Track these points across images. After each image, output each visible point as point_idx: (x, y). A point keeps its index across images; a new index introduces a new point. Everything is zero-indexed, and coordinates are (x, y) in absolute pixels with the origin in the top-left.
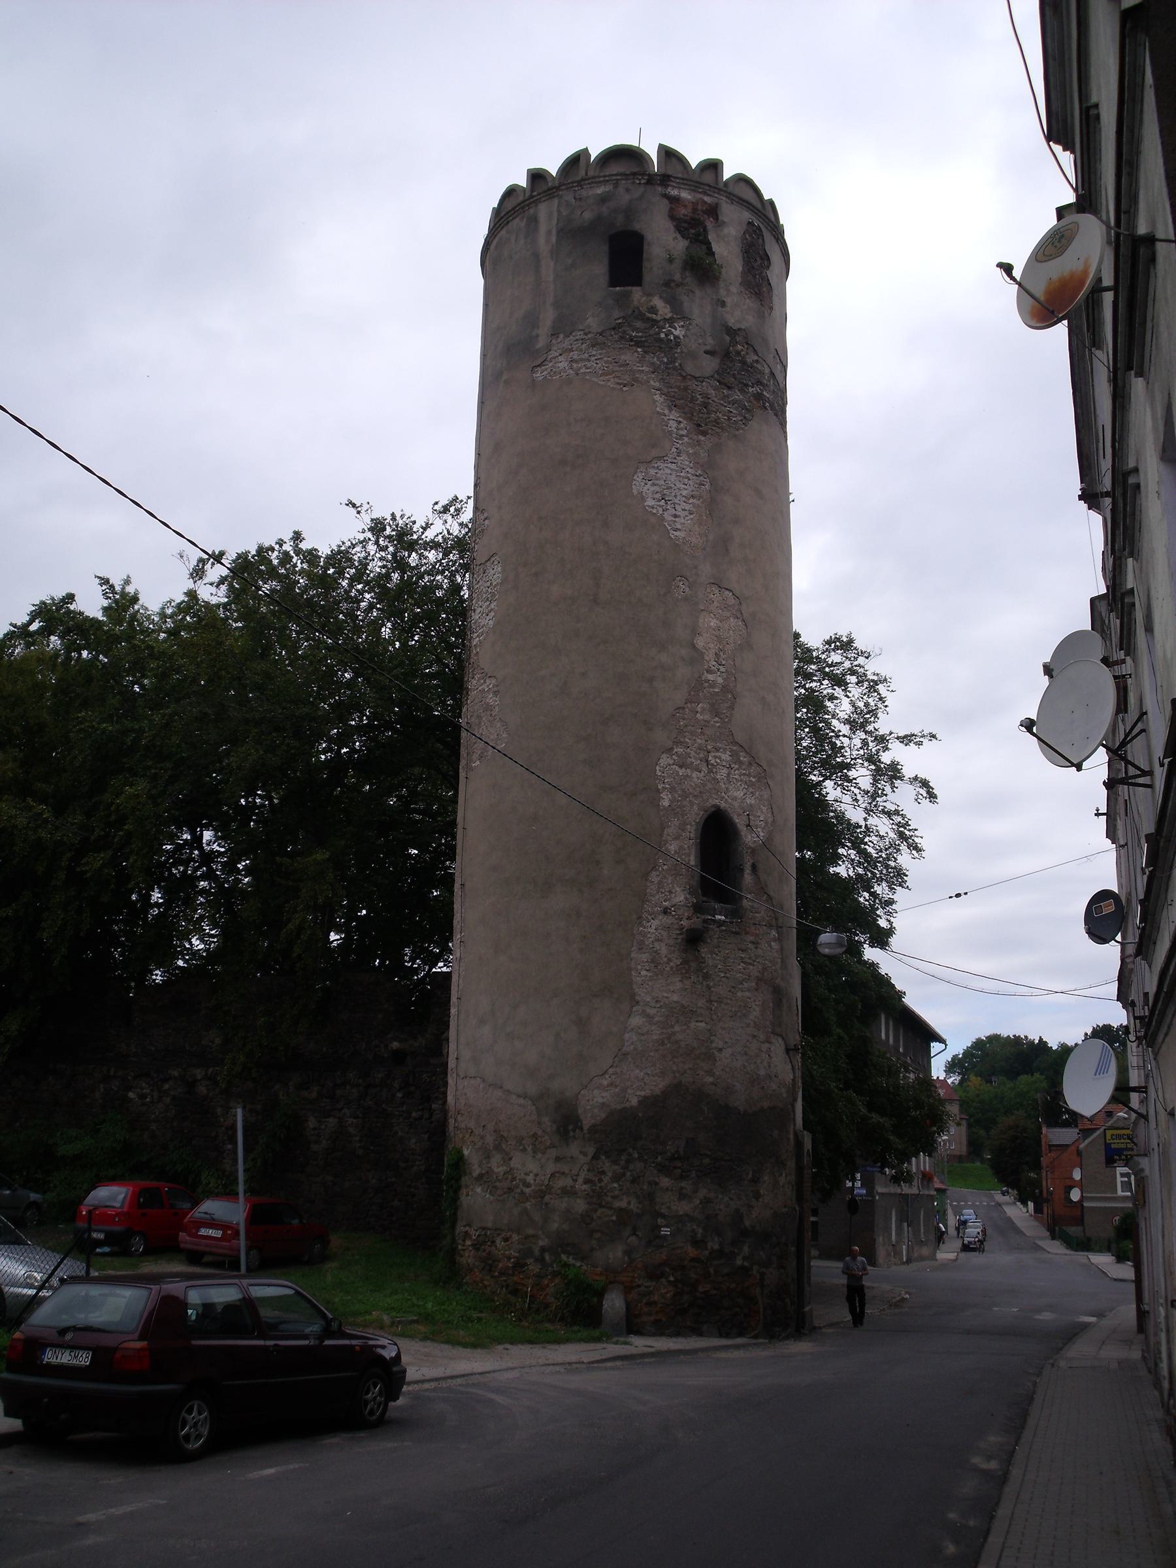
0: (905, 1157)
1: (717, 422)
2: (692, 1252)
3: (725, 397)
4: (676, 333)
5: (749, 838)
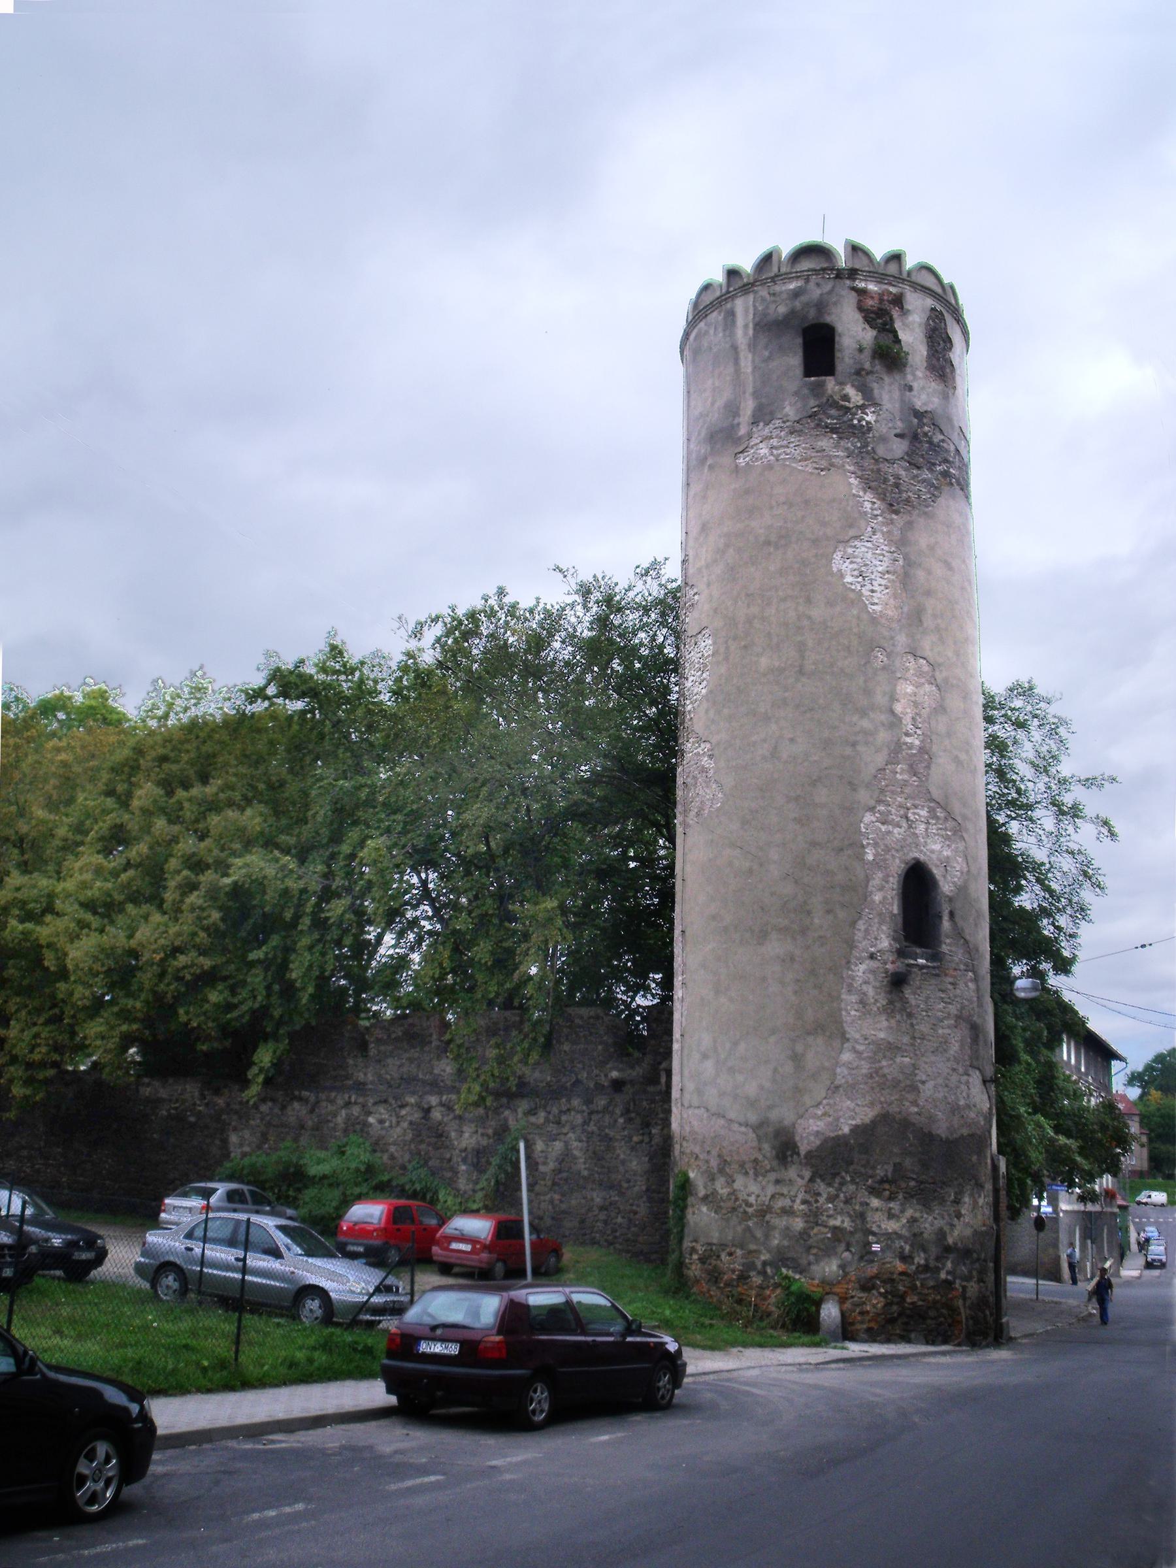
0: (1091, 1177)
1: (908, 501)
2: (900, 1266)
3: (915, 477)
4: (868, 418)
5: (946, 887)
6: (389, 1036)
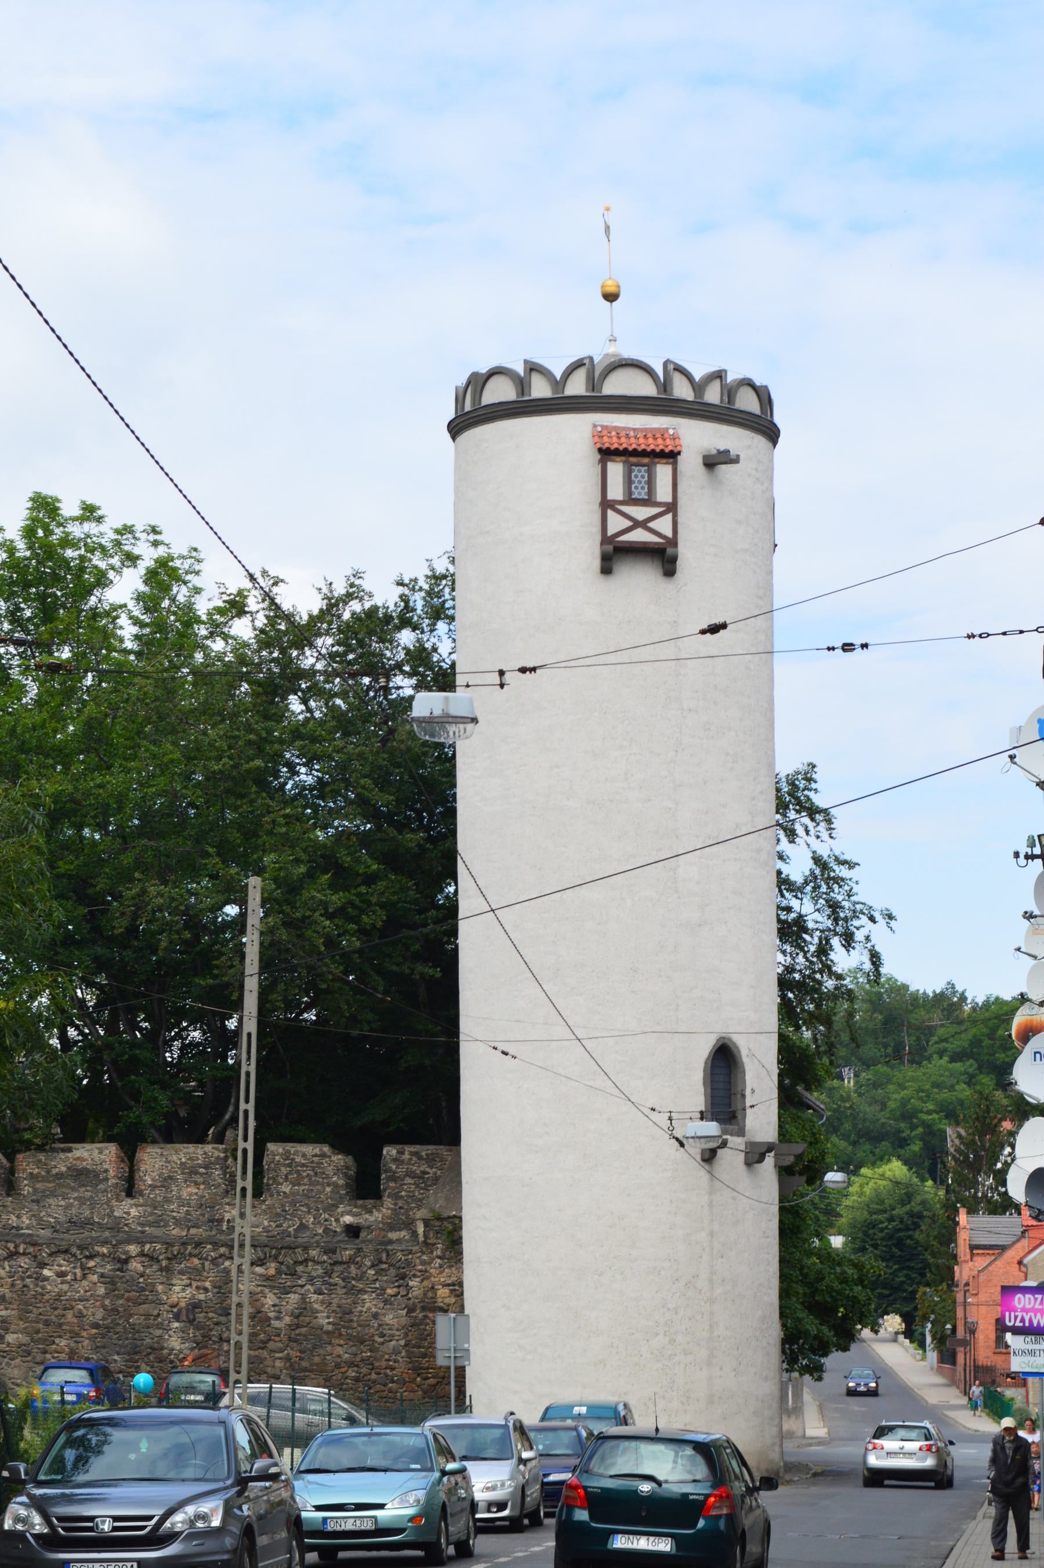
6: (48, 1172)
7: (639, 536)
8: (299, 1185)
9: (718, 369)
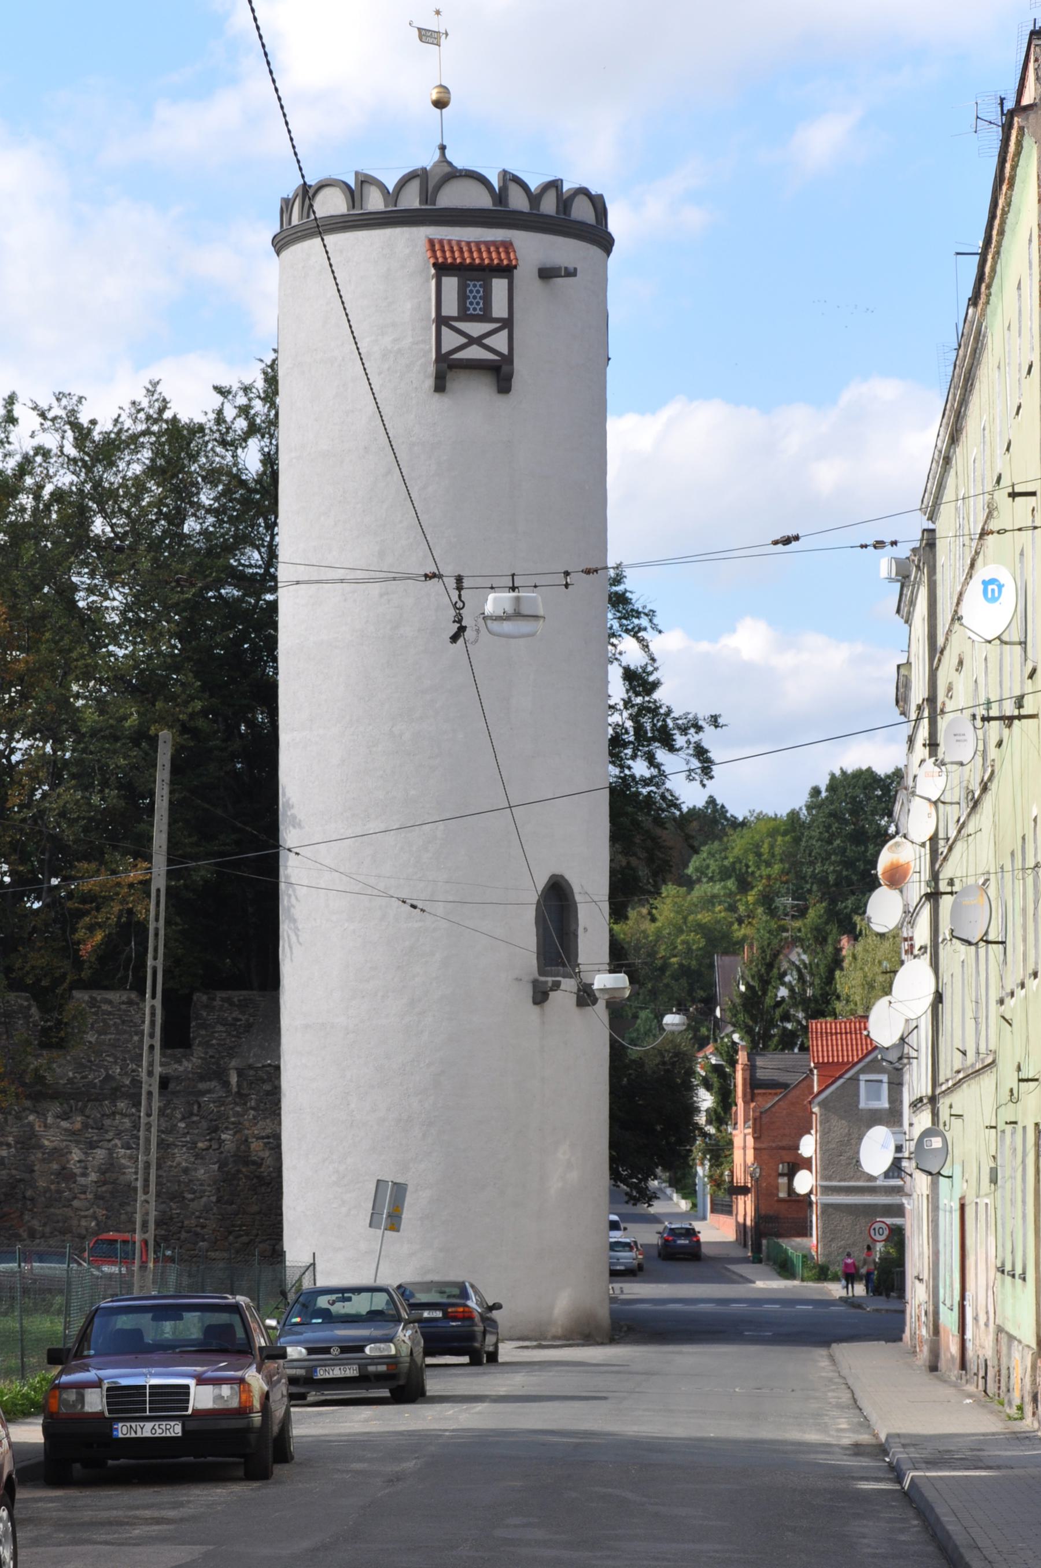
7: (474, 353)
8: (106, 1034)
9: (554, 178)
